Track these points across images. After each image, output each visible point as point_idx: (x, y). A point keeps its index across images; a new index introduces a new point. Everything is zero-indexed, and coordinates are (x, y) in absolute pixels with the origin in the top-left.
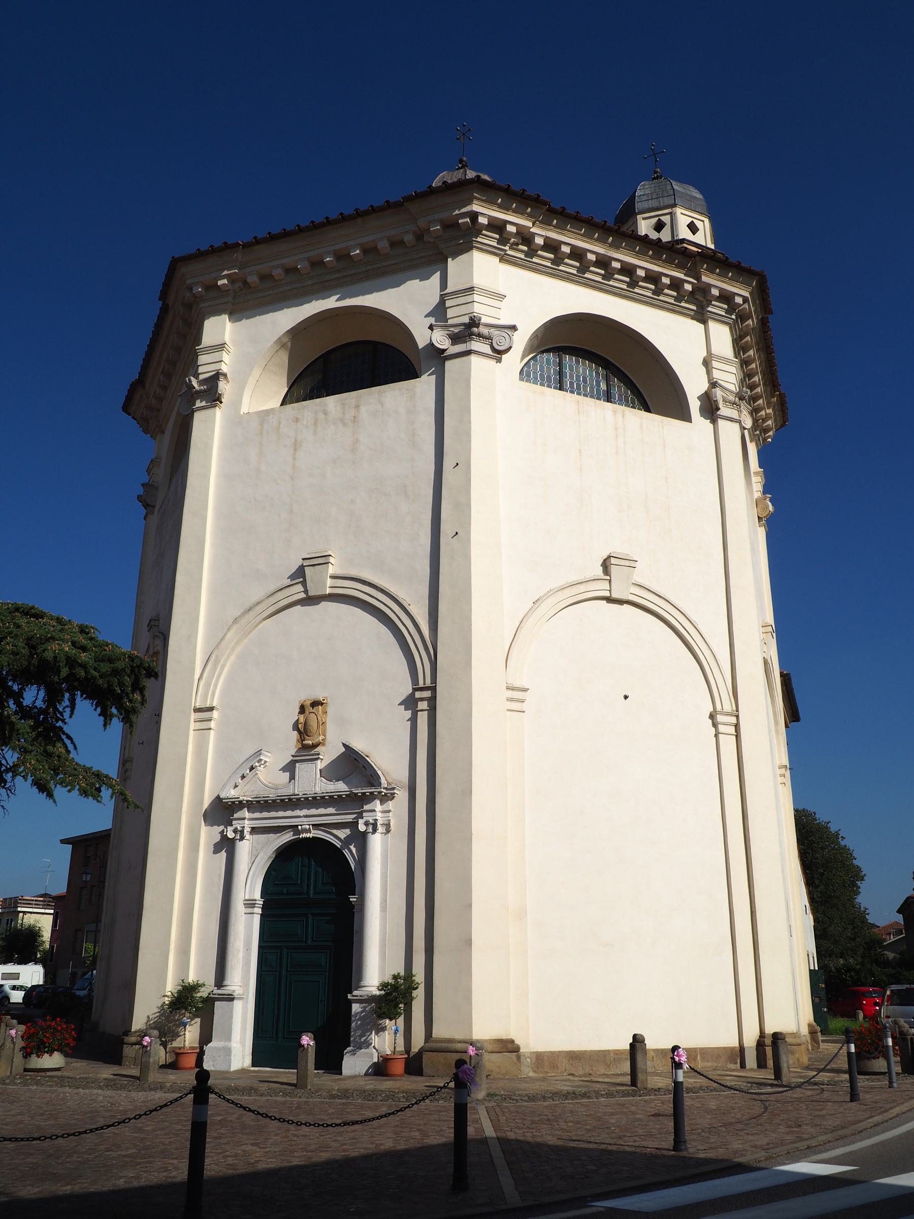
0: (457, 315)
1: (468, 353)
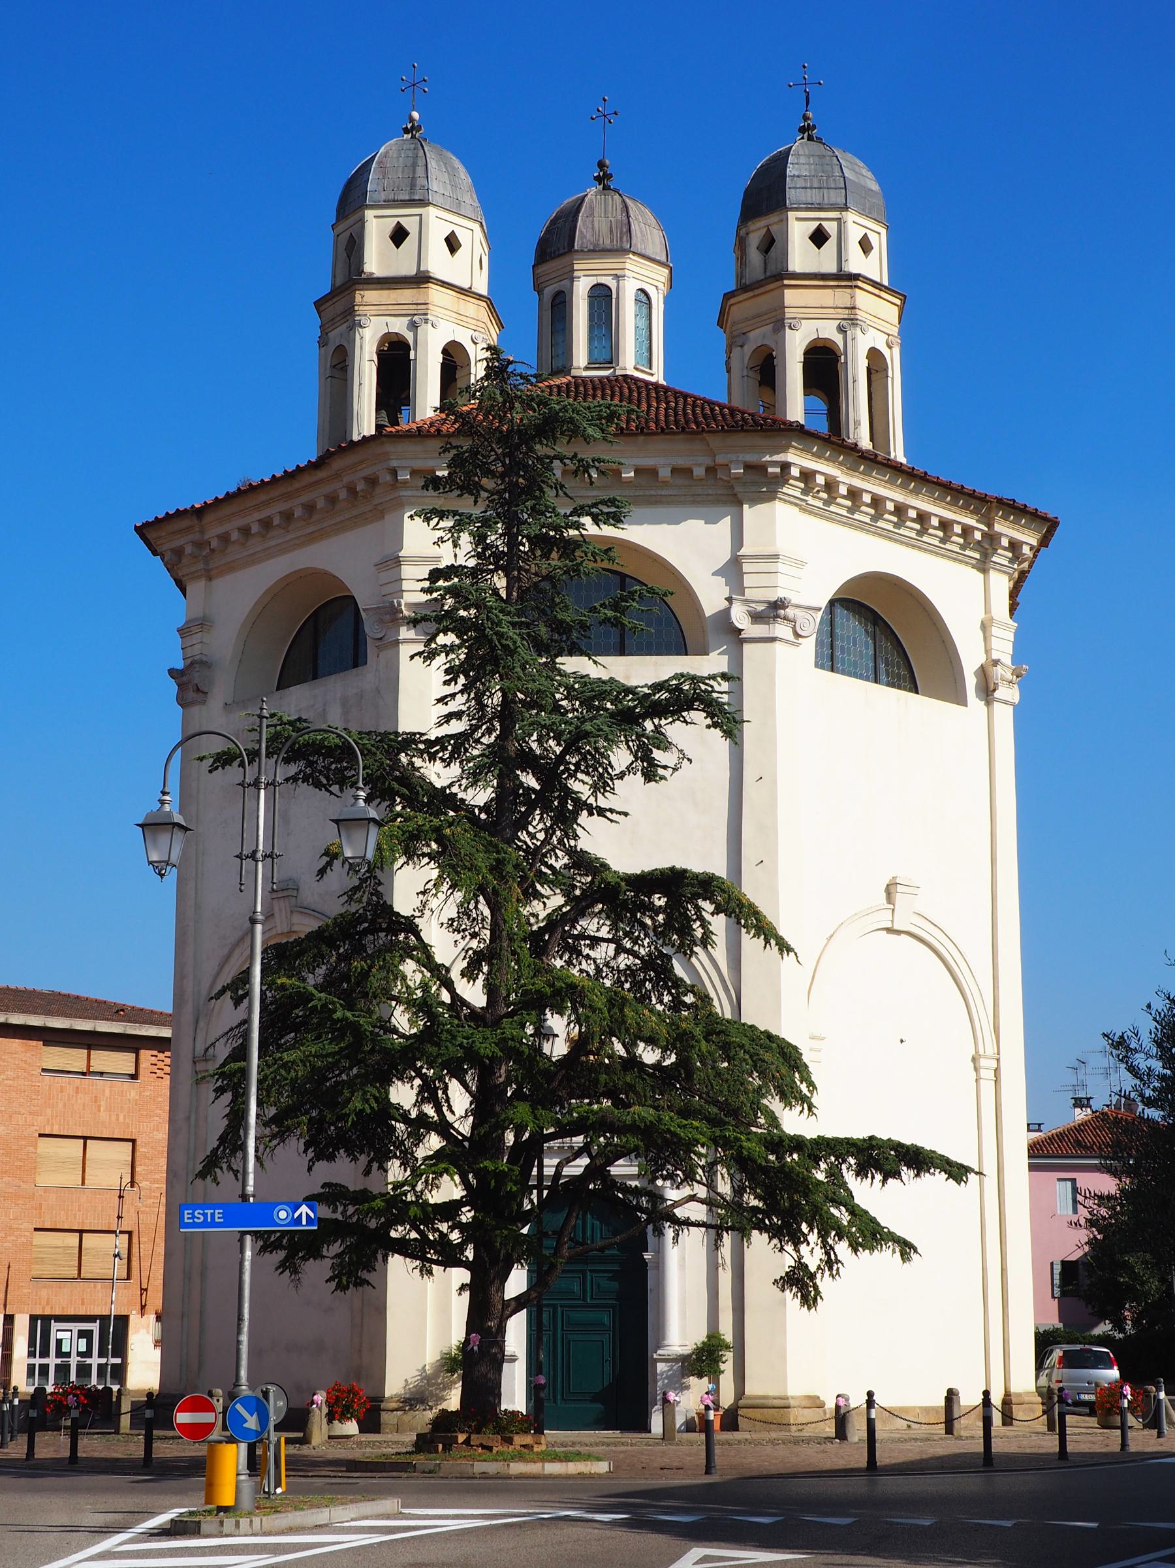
0: (758, 587)
1: (773, 640)
